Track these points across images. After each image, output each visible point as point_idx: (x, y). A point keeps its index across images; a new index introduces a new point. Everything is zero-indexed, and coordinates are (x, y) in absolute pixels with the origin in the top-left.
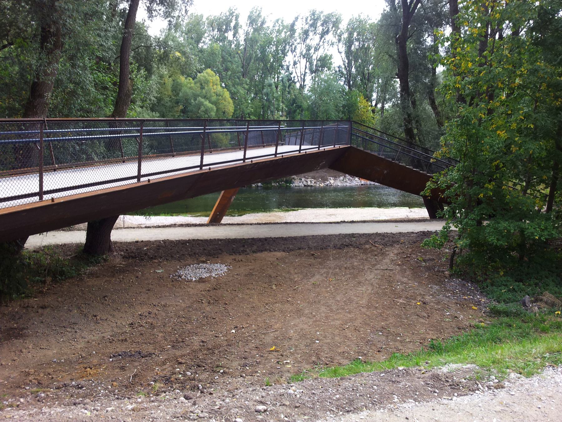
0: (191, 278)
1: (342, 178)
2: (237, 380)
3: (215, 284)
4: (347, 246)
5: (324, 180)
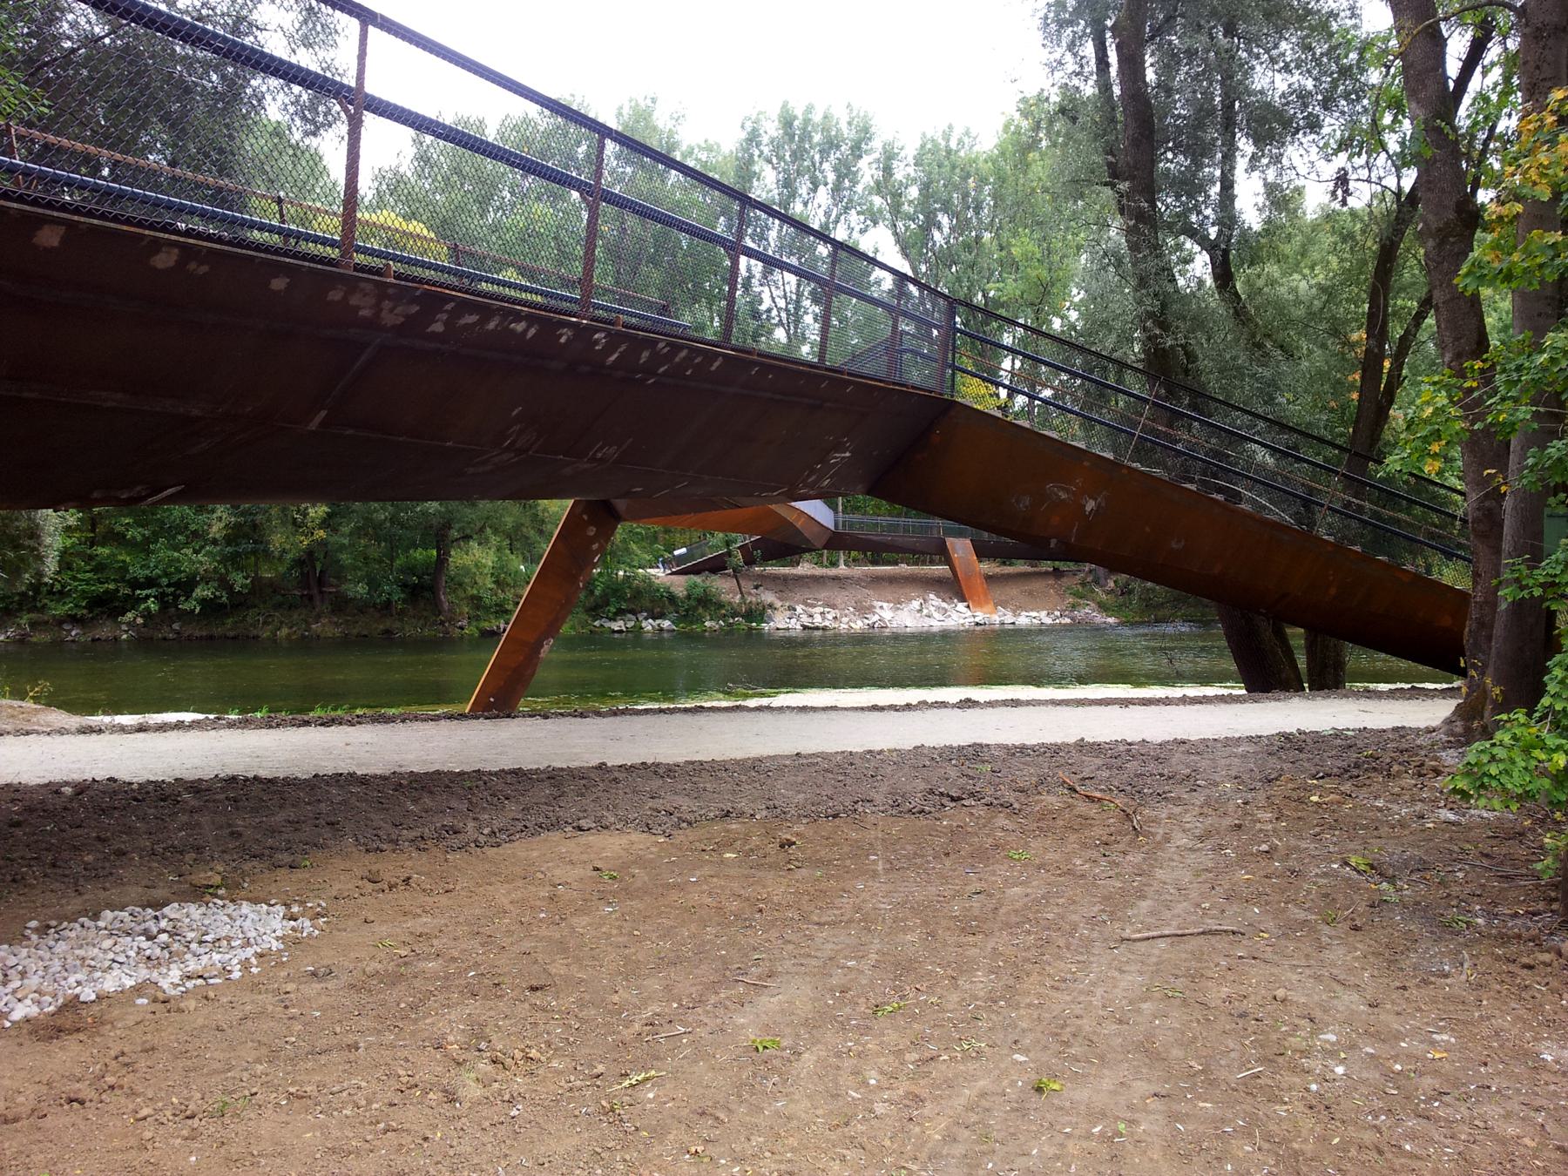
1: (916, 604)
4: (953, 799)
5: (863, 610)
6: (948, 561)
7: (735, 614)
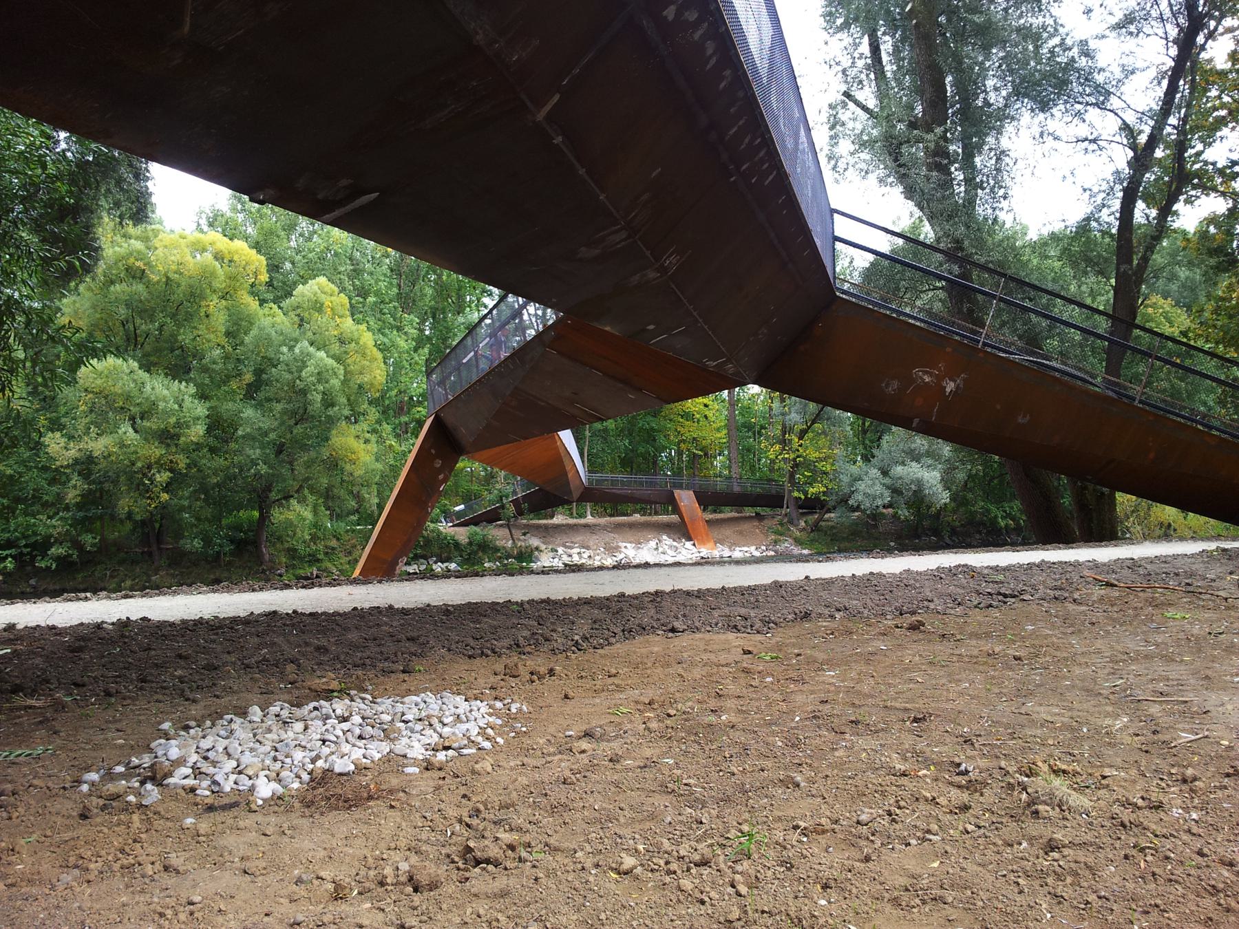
0: (245, 783)
1: (653, 544)
2: (267, 819)
3: (452, 812)
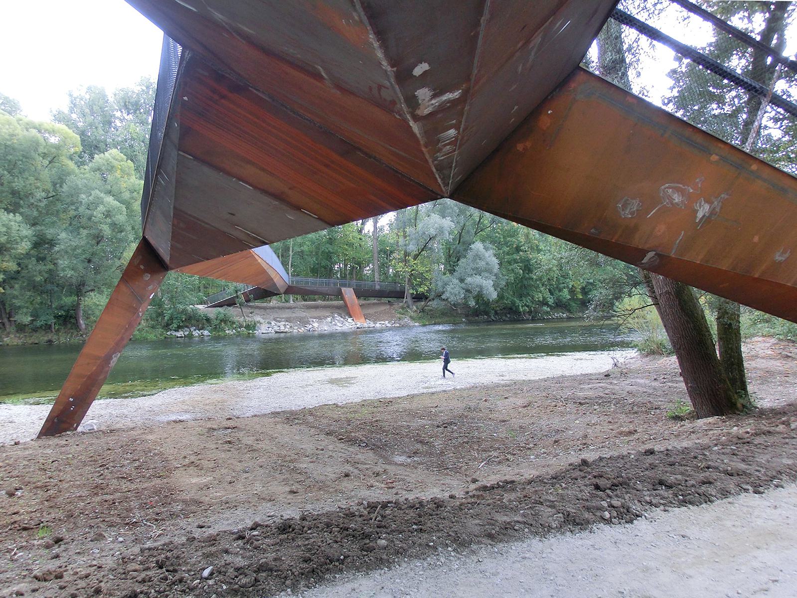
6: (343, 299)
7: (241, 327)
